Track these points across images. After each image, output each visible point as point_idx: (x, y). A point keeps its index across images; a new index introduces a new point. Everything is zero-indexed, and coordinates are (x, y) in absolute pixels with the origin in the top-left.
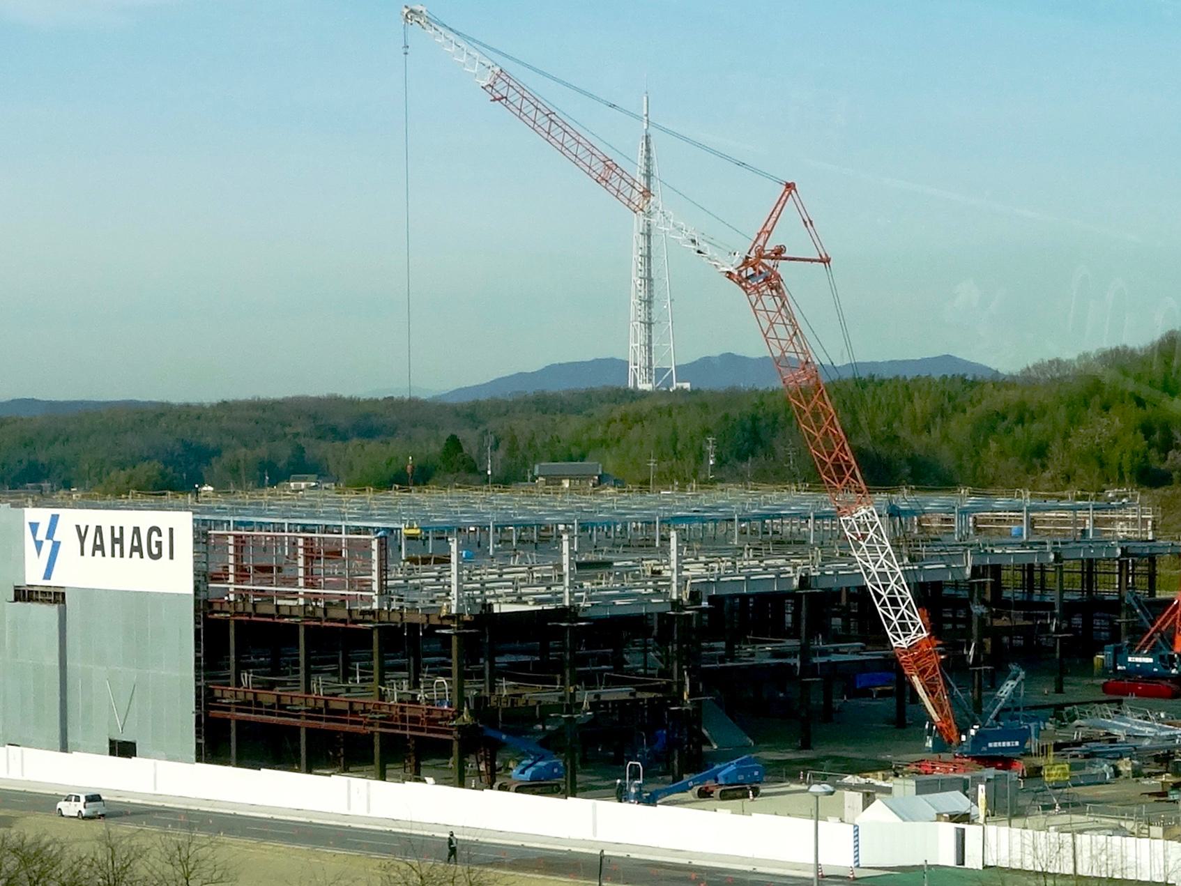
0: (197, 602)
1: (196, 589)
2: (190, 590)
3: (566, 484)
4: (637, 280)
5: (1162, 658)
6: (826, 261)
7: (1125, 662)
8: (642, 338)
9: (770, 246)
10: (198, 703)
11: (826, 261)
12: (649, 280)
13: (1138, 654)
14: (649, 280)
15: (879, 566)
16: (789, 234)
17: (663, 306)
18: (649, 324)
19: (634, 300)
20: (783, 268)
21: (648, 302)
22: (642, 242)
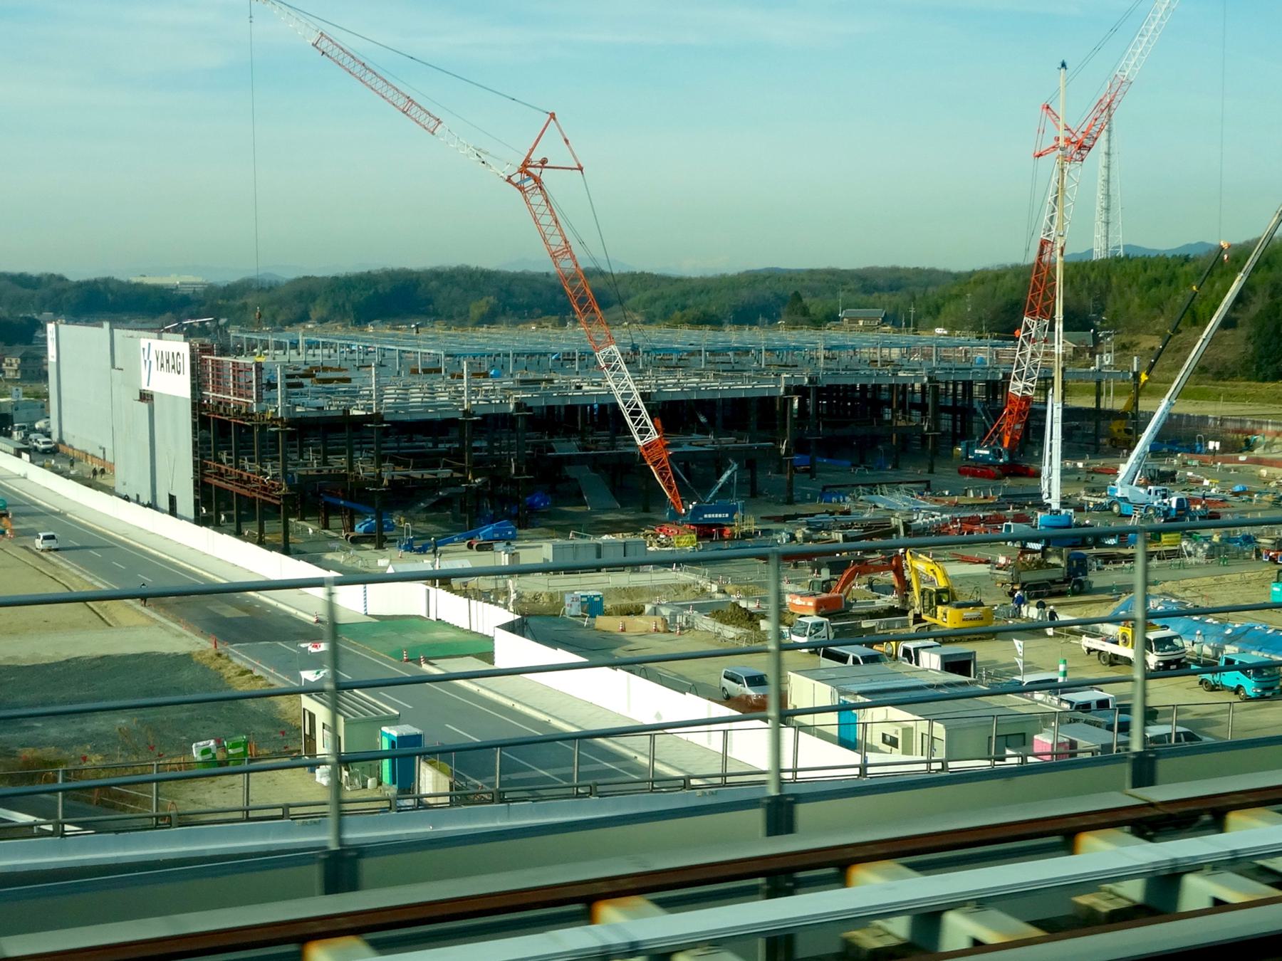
0: (194, 405)
1: (193, 395)
2: (189, 396)
3: (861, 323)
4: (1100, 195)
5: (994, 451)
6: (581, 169)
7: (973, 454)
8: (1103, 231)
9: (536, 158)
10: (195, 472)
11: (581, 169)
12: (1108, 196)
13: (981, 448)
14: (1108, 196)
15: (623, 387)
16: (551, 149)
17: (1117, 211)
18: (1108, 223)
19: (1098, 208)
20: (546, 176)
21: (1108, 209)
22: (1104, 172)
